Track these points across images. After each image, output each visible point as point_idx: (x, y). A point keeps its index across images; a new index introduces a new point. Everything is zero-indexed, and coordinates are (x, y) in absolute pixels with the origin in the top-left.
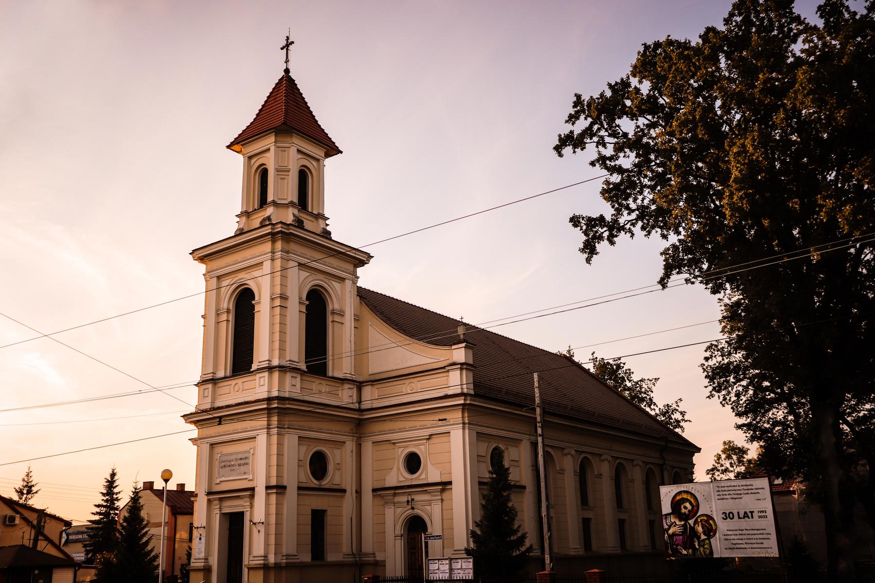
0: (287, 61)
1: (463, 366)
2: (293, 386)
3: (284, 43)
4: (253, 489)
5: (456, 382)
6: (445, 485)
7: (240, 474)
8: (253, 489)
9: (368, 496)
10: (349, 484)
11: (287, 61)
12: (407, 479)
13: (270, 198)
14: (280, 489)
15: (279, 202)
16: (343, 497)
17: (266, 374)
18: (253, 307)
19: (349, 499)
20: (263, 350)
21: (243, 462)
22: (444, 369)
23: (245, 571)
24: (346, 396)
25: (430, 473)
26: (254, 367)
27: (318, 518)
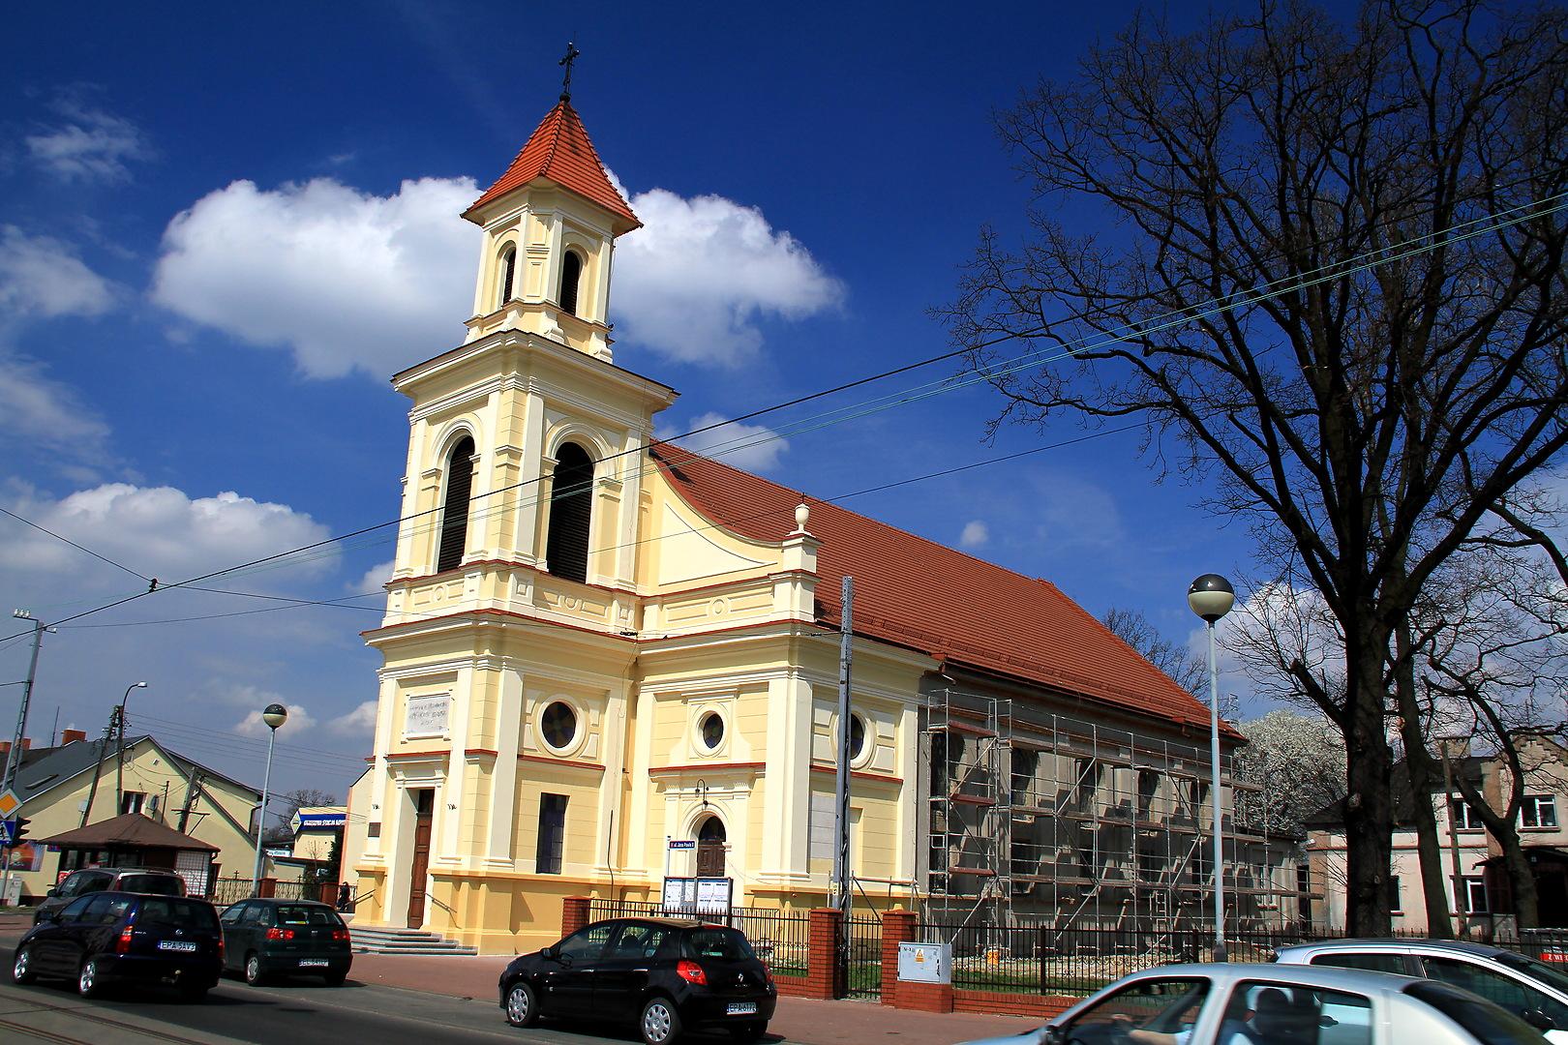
0: (566, 82)
1: (797, 576)
2: (514, 597)
3: (566, 54)
4: (448, 753)
5: (793, 603)
6: (754, 770)
7: (433, 729)
8: (448, 753)
9: (640, 779)
10: (607, 755)
11: (566, 82)
12: (701, 756)
13: (514, 296)
14: (484, 757)
15: (527, 300)
16: (598, 782)
17: (492, 576)
18: (471, 464)
19: (612, 780)
20: (479, 541)
21: (438, 710)
22: (768, 581)
23: (430, 879)
24: (614, 619)
25: (734, 748)
26: (465, 560)
27: (553, 809)
